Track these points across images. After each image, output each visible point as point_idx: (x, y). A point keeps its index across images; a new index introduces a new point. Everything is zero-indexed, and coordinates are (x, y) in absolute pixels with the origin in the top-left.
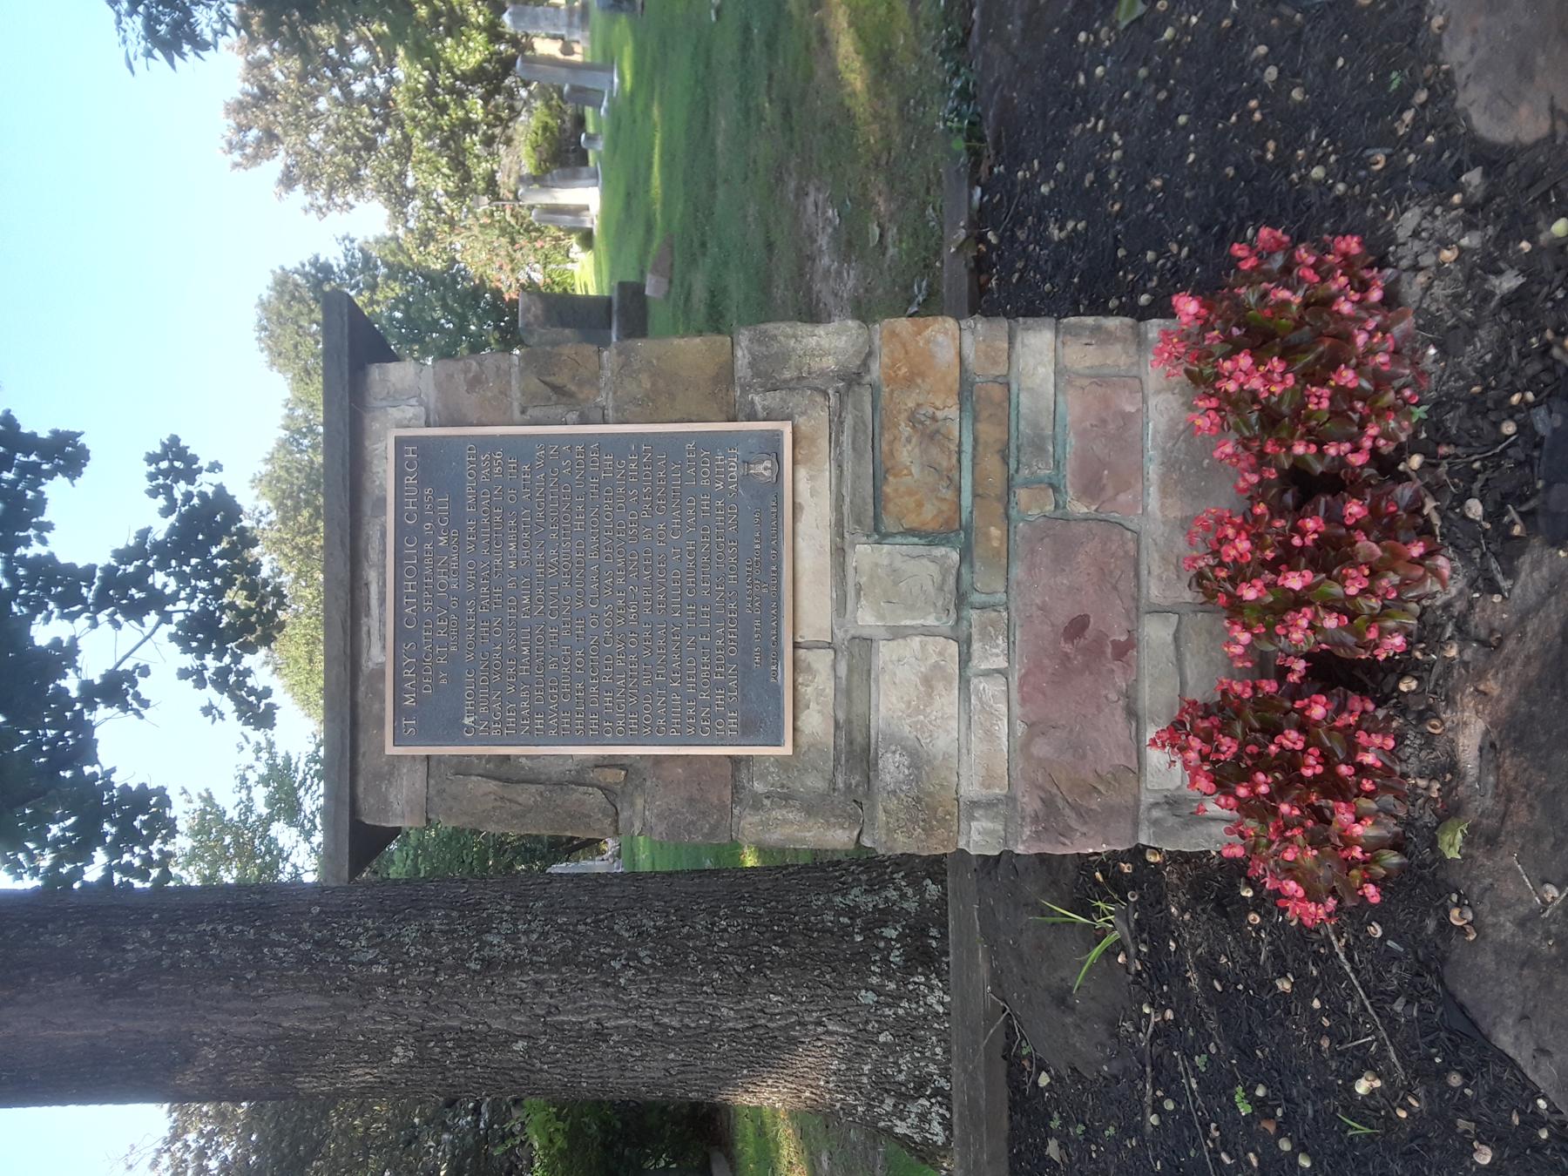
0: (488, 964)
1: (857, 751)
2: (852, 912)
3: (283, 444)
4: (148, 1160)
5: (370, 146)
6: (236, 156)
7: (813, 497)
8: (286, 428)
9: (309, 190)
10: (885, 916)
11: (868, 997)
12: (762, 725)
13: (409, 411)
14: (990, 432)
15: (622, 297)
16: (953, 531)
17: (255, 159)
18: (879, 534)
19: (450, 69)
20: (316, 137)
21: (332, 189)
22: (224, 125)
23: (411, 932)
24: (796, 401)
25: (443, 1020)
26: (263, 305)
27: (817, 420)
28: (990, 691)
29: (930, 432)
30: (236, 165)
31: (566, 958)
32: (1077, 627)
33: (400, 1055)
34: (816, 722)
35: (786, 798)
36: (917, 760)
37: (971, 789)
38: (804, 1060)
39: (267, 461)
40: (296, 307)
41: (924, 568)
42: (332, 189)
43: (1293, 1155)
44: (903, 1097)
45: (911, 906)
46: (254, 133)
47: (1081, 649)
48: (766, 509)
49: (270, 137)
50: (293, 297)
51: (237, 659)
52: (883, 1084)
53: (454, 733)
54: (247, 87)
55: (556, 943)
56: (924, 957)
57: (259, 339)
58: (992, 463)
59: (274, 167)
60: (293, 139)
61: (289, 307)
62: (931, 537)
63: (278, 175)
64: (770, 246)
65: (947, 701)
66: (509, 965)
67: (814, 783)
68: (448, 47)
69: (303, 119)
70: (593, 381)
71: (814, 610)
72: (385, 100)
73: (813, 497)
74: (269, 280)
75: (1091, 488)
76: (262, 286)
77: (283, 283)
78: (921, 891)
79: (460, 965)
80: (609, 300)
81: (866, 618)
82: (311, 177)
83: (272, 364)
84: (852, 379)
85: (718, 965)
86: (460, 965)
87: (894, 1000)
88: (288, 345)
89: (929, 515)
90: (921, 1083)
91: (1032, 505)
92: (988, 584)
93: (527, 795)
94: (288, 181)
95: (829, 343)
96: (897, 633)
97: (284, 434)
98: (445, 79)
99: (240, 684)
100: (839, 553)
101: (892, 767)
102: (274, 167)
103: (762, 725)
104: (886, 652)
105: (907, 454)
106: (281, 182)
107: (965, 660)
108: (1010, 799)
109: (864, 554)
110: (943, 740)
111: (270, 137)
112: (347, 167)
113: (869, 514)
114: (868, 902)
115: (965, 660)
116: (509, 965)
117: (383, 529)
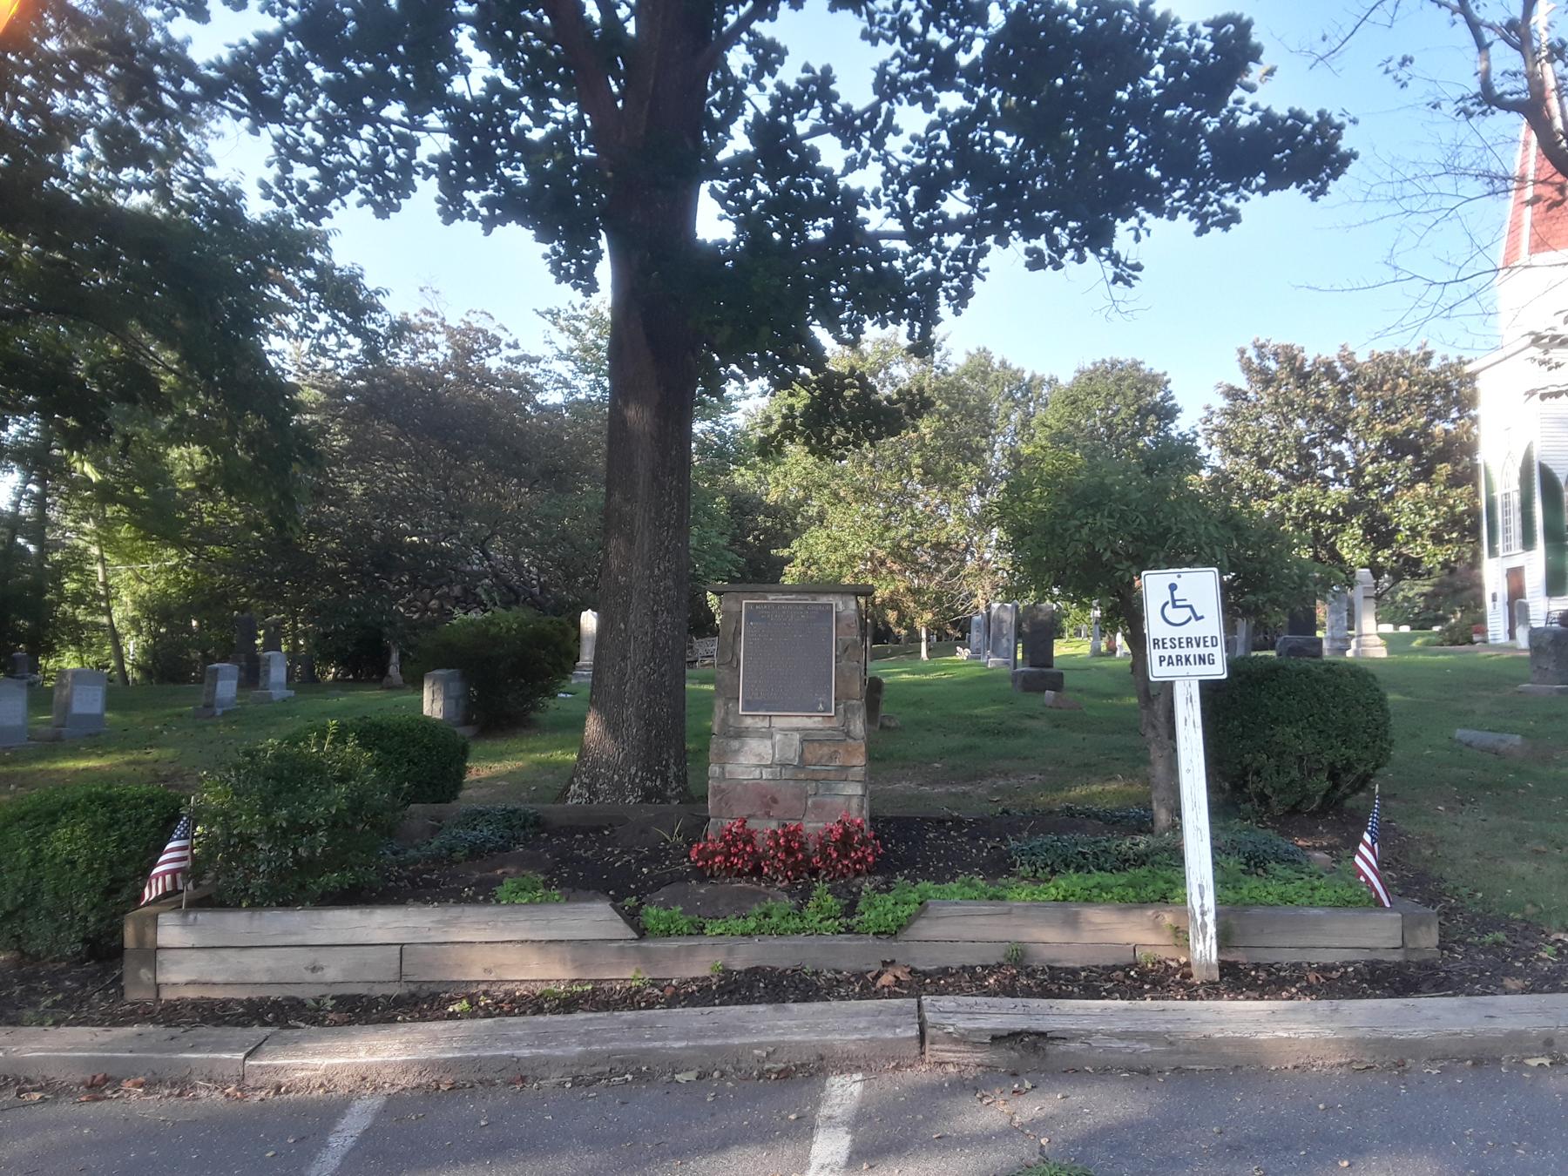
0: (656, 614)
1: (740, 734)
2: (667, 767)
3: (1017, 375)
4: (429, 308)
5: (1263, 463)
6: (1251, 353)
7: (812, 722)
8: (1031, 380)
9: (1224, 413)
10: (665, 781)
11: (633, 770)
12: (748, 705)
13: (841, 607)
14: (832, 776)
15: (1053, 675)
16: (803, 764)
17: (1247, 367)
18: (802, 741)
19: (1335, 532)
20: (1268, 421)
21: (1223, 432)
22: (1278, 339)
23: (670, 583)
24: (841, 717)
25: (635, 596)
26: (1136, 365)
27: (835, 723)
28: (757, 774)
29: (832, 757)
30: (1242, 352)
31: (656, 644)
32: (775, 801)
33: (622, 579)
34: (749, 722)
35: (727, 714)
36: (737, 751)
37: (728, 767)
38: (608, 743)
39: (1003, 364)
40: (1131, 393)
41: (792, 755)
42: (1223, 432)
43: (1076, 149)
44: (589, 787)
45: (669, 793)
46: (1273, 365)
47: (769, 802)
48: (809, 708)
49: (1267, 380)
50: (1139, 391)
51: (801, 434)
52: (595, 779)
53: (748, 619)
54: (1310, 362)
55: (661, 641)
56: (648, 796)
57: (1104, 361)
58: (823, 775)
59: (1241, 382)
60: (1266, 400)
61: (1130, 387)
62: (801, 756)
63: (1237, 386)
64: (1026, 758)
65: (754, 761)
66: (655, 622)
67: (731, 721)
68: (1355, 530)
69: (1285, 408)
70: (849, 659)
71: (778, 723)
72: (1309, 474)
73: (812, 722)
74: (1158, 370)
75: (815, 805)
76: (1153, 363)
77: (1156, 381)
78: (675, 798)
79: (655, 602)
80: (1051, 666)
81: (778, 737)
82: (1234, 415)
83: (1082, 373)
84: (848, 734)
85: (649, 707)
86: (655, 602)
87: (632, 782)
88: (1098, 387)
89: (808, 756)
90: (594, 794)
91: (810, 788)
92: (787, 774)
93: (730, 639)
94: (1233, 394)
95: (858, 726)
96: (773, 747)
97: (1027, 376)
98: (1326, 528)
99: (785, 437)
100: (797, 730)
101: (735, 744)
102: (1241, 382)
103: (748, 705)
104: (768, 743)
105: (825, 750)
106: (1232, 388)
107: (766, 766)
108: (725, 779)
109: (797, 736)
110: (742, 760)
111: (1267, 380)
112: (1241, 445)
113: (808, 738)
114: (671, 774)
115: (766, 766)
116: (655, 622)
117: (807, 600)
